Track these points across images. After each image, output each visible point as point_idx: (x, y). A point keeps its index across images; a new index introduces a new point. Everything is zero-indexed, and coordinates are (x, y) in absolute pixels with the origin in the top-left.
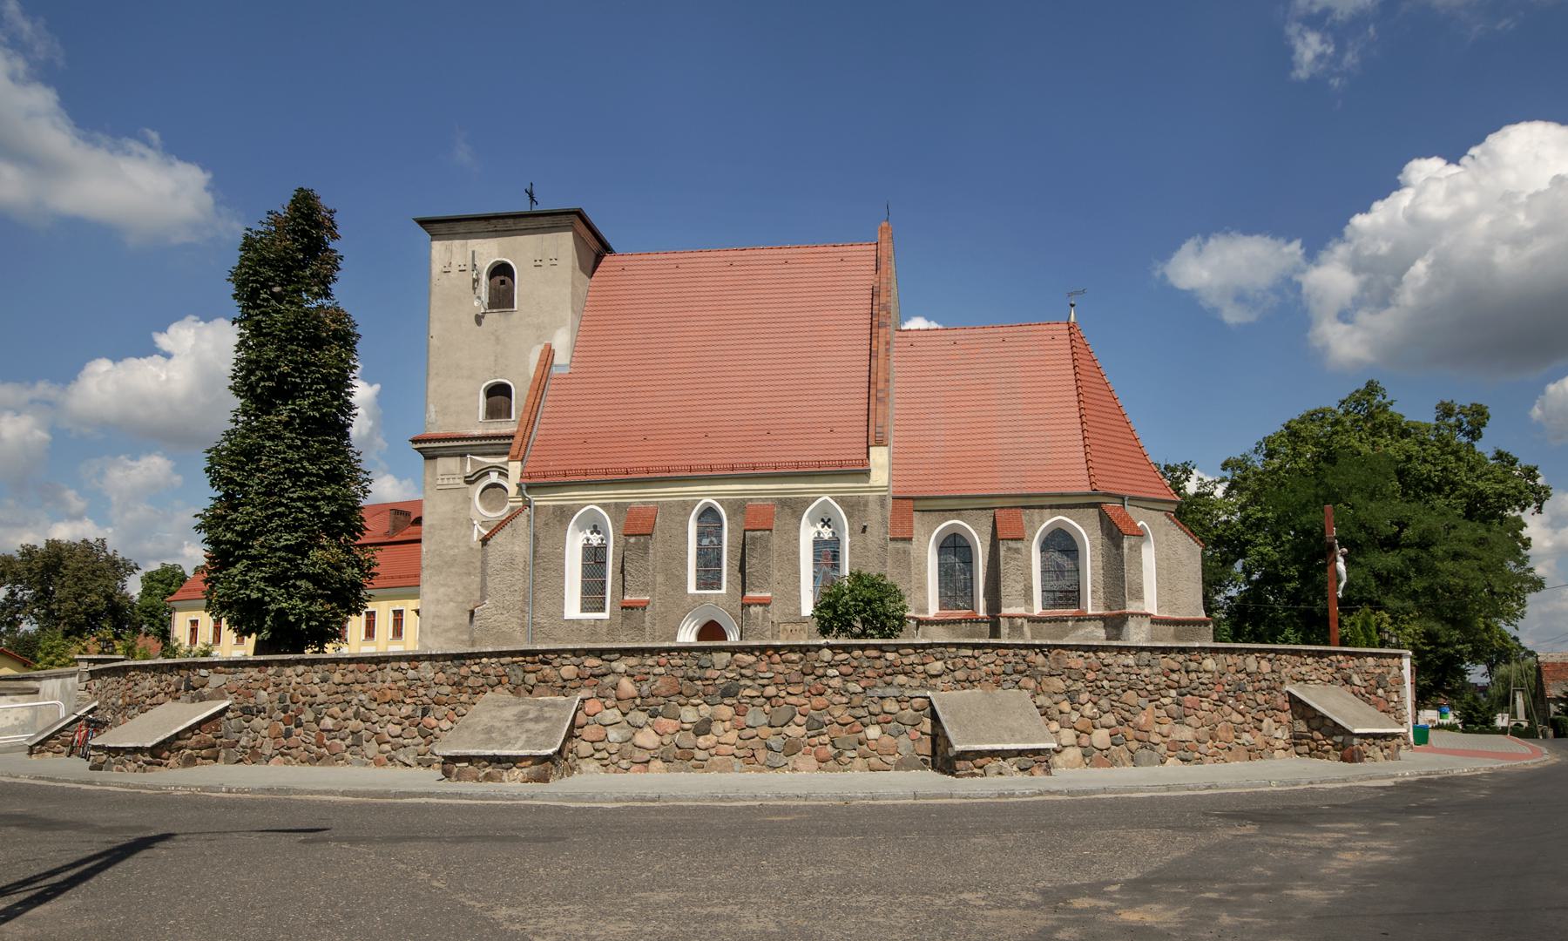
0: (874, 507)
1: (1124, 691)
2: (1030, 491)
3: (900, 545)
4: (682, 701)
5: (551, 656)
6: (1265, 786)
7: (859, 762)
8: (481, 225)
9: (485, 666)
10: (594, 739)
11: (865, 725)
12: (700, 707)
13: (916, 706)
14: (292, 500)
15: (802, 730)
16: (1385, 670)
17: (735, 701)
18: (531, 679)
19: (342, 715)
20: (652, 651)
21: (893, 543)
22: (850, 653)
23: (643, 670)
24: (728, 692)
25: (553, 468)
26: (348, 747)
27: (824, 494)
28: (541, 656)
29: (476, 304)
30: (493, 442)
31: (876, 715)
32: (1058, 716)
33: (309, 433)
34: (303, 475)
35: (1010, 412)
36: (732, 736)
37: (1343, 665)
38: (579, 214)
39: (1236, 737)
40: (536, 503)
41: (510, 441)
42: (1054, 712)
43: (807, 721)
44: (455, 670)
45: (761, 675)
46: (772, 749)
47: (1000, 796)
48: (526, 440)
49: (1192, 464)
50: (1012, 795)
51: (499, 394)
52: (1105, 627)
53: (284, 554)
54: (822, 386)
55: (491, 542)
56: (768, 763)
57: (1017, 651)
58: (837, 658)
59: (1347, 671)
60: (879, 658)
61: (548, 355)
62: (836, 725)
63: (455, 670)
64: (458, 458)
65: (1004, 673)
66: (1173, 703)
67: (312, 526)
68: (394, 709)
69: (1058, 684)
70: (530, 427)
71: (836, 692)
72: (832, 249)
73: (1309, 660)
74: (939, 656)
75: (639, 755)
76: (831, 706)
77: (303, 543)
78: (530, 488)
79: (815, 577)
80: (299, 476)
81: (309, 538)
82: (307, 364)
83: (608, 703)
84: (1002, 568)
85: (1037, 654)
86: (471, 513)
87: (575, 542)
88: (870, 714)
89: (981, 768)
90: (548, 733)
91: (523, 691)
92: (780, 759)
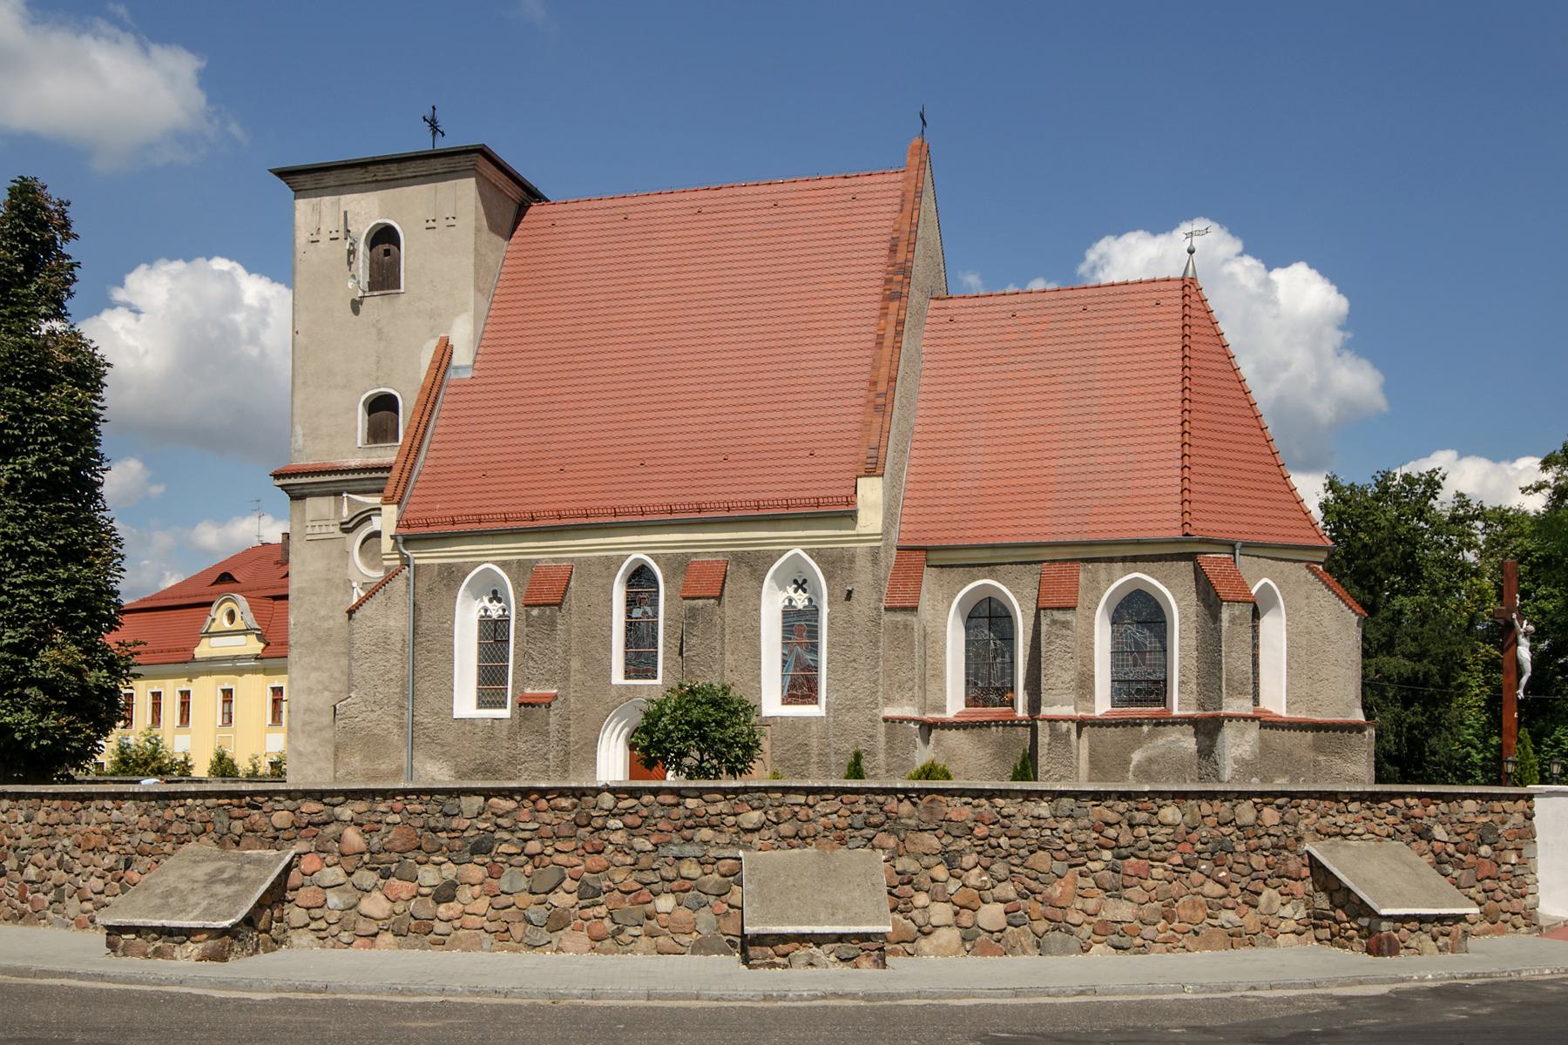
0: (862, 563)
1: (1032, 852)
2: (1092, 537)
3: (900, 617)
4: (421, 858)
5: (260, 799)
6: (1174, 991)
7: (644, 941)
8: (356, 174)
9: (191, 809)
10: (310, 905)
11: (656, 894)
12: (443, 867)
13: (723, 870)
14: (16, 586)
15: (573, 899)
16: (1496, 818)
17: (487, 860)
18: (238, 826)
19: (46, 863)
20: (386, 794)
21: (889, 614)
22: (638, 799)
23: (373, 818)
24: (481, 847)
25: (440, 513)
26: (51, 903)
28: (248, 799)
29: (350, 285)
30: (374, 475)
31: (670, 881)
32: (928, 885)
33: (36, 499)
34: (27, 554)
35: (1080, 419)
36: (482, 905)
37: (1417, 811)
38: (483, 152)
39: (1209, 917)
40: (417, 562)
41: (385, 474)
42: (923, 879)
43: (580, 887)
44: (159, 812)
45: (522, 826)
46: (530, 922)
47: (766, 998)
48: (405, 475)
49: (1441, 473)
50: (783, 998)
51: (382, 406)
52: (1196, 734)
53: (7, 655)
54: (806, 388)
55: (357, 615)
56: (526, 940)
57: (871, 797)
58: (621, 805)
59: (1425, 821)
60: (677, 805)
62: (616, 892)
63: (159, 812)
64: (332, 498)
65: (851, 826)
66: (1106, 868)
67: (41, 619)
68: (97, 858)
69: (930, 841)
70: (412, 456)
71: (619, 849)
72: (840, 182)
73: (1354, 806)
74: (756, 804)
75: (365, 927)
76: (612, 868)
77: (29, 641)
78: (408, 541)
79: (784, 662)
80: (23, 556)
81: (39, 635)
82: (29, 410)
83: (329, 859)
84: (1043, 649)
85: (900, 801)
86: (350, 572)
87: (468, 615)
88: (663, 879)
89: (785, 956)
90: (235, 900)
91: (229, 843)
92: (542, 935)
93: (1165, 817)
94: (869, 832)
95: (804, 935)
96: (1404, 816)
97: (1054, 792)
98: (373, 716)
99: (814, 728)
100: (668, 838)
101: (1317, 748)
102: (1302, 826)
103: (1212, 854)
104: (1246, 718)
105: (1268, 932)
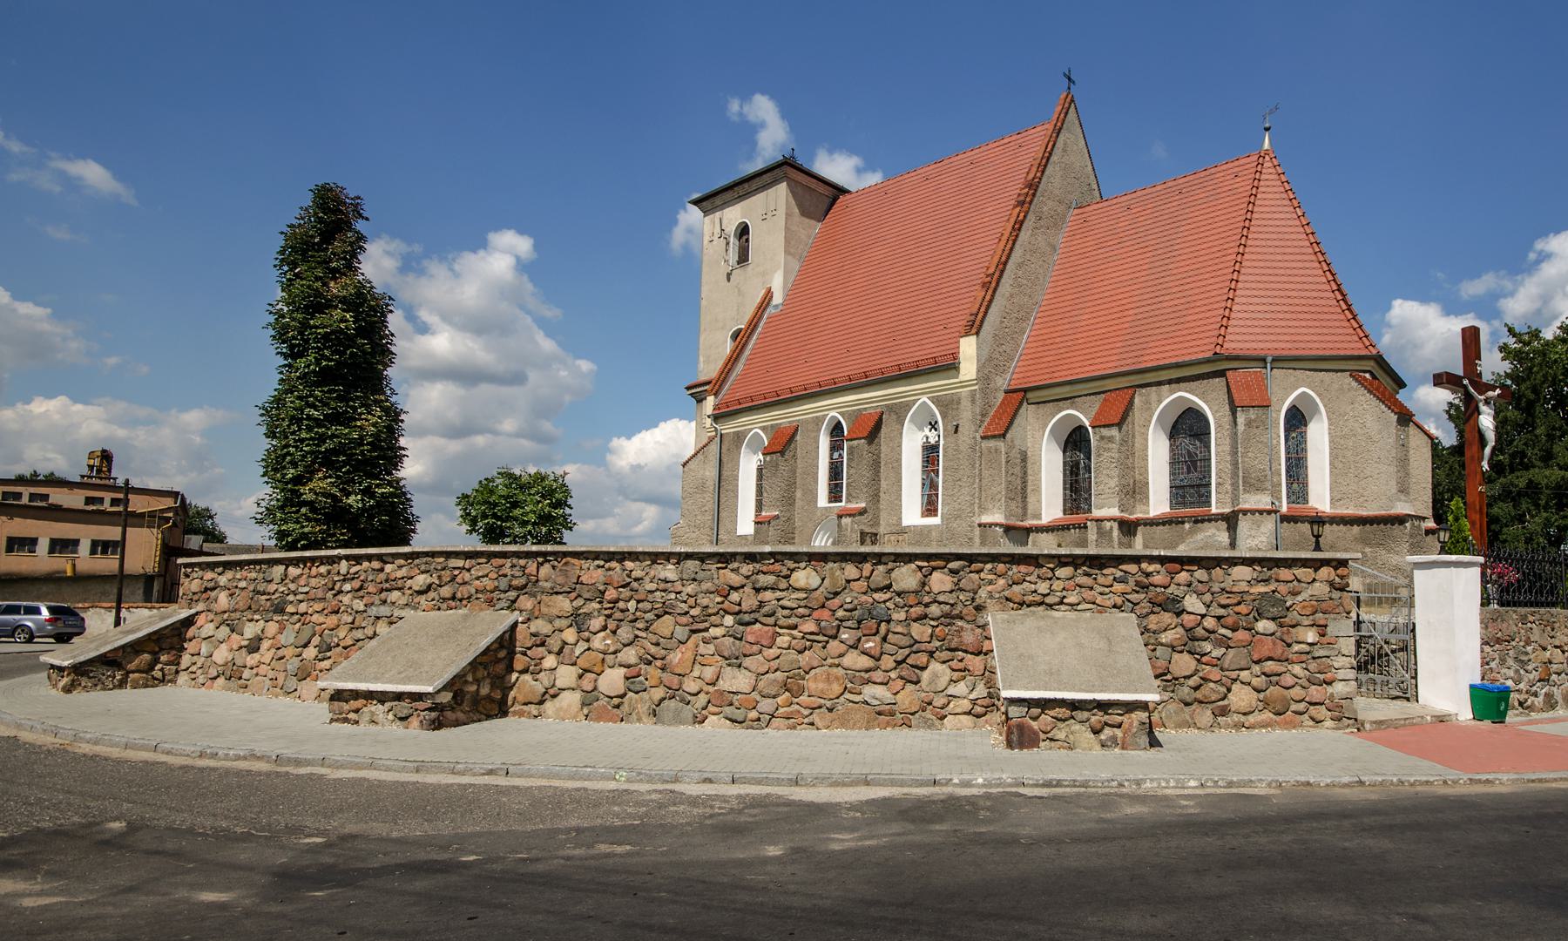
0: (966, 403)
1: (658, 617)
8: (728, 196)
16: (1283, 588)
27: (921, 394)
61: (769, 295)
65: (496, 588)
69: (564, 604)
73: (1064, 572)
79: (923, 484)
93: (797, 580)
94: (512, 594)
95: (371, 692)
96: (1137, 583)
97: (680, 554)
98: (694, 535)
99: (934, 534)
100: (372, 600)
101: (1365, 541)
102: (983, 593)
103: (859, 622)
104: (1261, 512)
105: (933, 711)
